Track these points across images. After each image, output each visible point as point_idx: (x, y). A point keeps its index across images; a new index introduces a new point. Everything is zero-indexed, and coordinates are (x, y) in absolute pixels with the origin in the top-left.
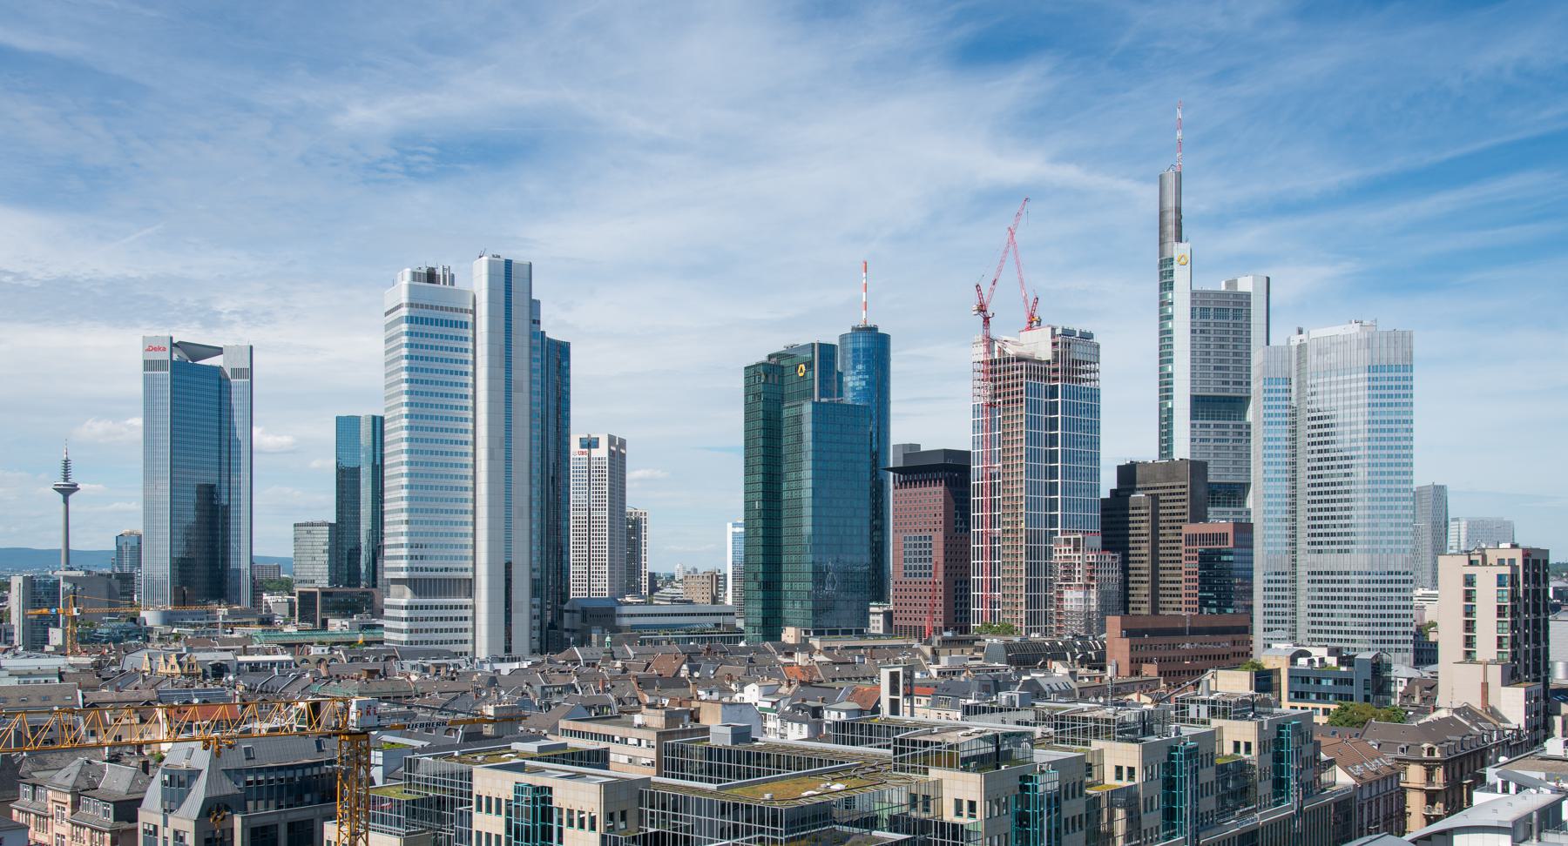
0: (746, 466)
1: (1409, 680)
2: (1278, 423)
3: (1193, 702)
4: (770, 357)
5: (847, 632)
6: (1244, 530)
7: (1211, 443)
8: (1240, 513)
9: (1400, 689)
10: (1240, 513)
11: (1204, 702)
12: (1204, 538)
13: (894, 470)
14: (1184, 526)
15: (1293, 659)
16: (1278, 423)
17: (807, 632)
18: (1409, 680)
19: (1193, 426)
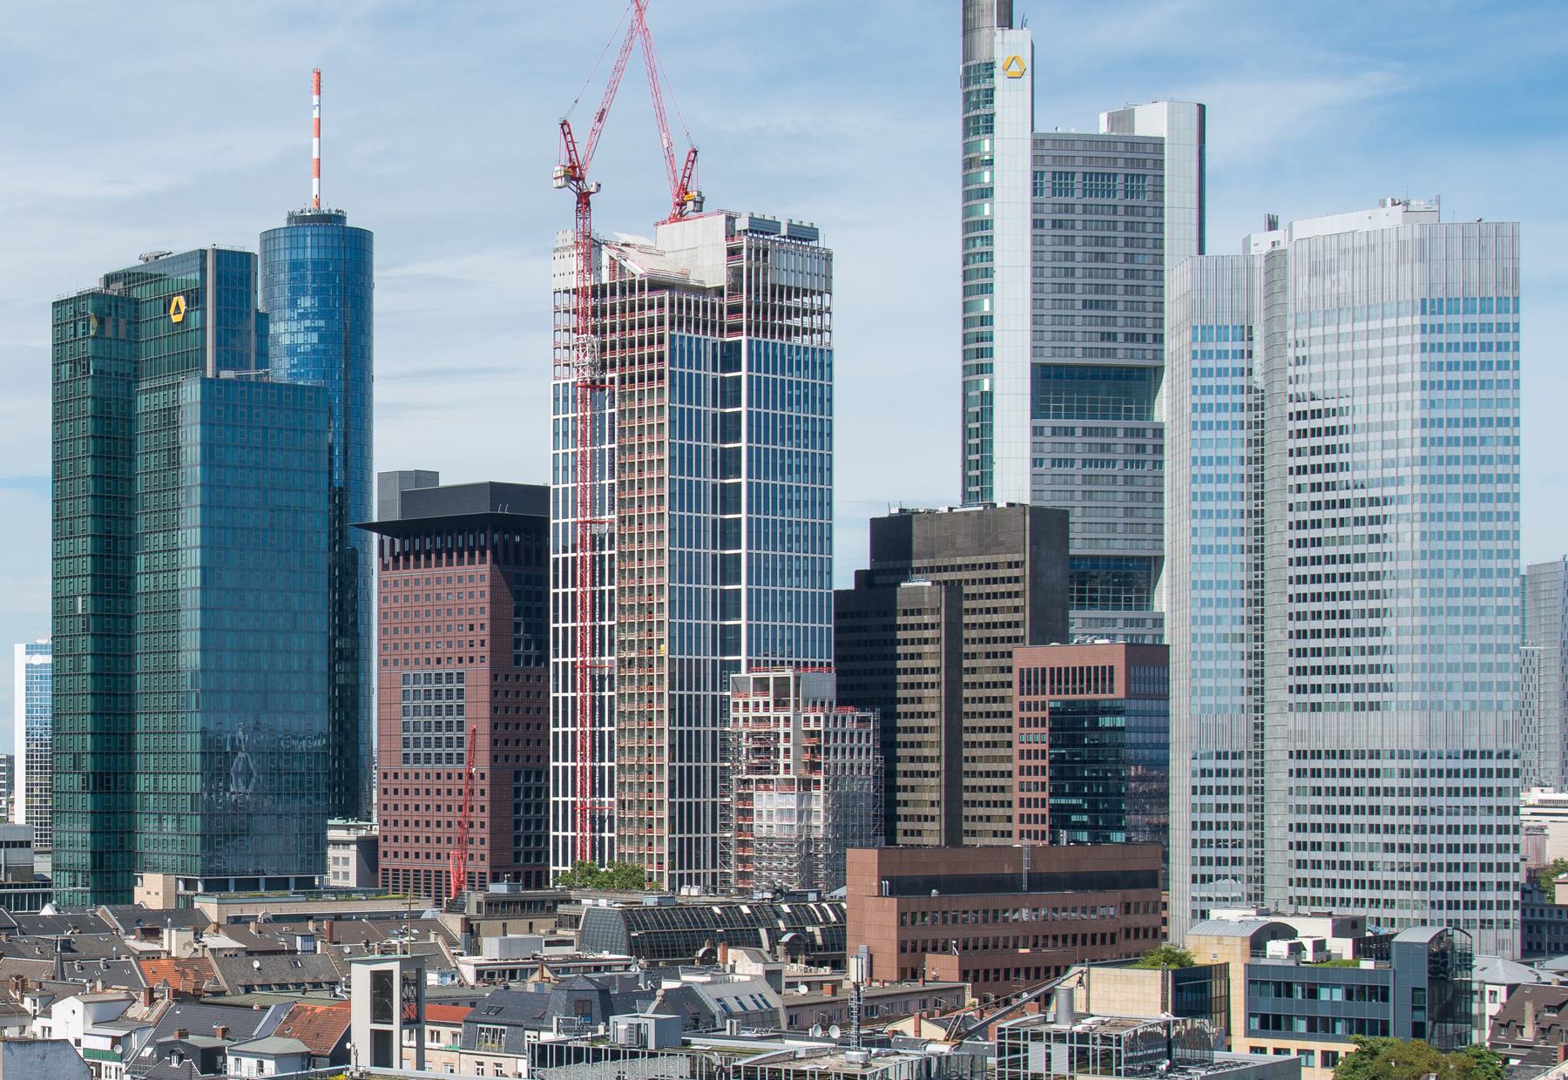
1: (1511, 989)
3: (1037, 1037)
4: (109, 279)
5: (278, 884)
6: (1149, 661)
7: (1077, 469)
8: (1139, 623)
9: (1492, 1009)
10: (1139, 623)
11: (1060, 1037)
12: (1061, 677)
13: (380, 528)
17: (189, 884)
18: (1511, 989)
19: (1036, 431)
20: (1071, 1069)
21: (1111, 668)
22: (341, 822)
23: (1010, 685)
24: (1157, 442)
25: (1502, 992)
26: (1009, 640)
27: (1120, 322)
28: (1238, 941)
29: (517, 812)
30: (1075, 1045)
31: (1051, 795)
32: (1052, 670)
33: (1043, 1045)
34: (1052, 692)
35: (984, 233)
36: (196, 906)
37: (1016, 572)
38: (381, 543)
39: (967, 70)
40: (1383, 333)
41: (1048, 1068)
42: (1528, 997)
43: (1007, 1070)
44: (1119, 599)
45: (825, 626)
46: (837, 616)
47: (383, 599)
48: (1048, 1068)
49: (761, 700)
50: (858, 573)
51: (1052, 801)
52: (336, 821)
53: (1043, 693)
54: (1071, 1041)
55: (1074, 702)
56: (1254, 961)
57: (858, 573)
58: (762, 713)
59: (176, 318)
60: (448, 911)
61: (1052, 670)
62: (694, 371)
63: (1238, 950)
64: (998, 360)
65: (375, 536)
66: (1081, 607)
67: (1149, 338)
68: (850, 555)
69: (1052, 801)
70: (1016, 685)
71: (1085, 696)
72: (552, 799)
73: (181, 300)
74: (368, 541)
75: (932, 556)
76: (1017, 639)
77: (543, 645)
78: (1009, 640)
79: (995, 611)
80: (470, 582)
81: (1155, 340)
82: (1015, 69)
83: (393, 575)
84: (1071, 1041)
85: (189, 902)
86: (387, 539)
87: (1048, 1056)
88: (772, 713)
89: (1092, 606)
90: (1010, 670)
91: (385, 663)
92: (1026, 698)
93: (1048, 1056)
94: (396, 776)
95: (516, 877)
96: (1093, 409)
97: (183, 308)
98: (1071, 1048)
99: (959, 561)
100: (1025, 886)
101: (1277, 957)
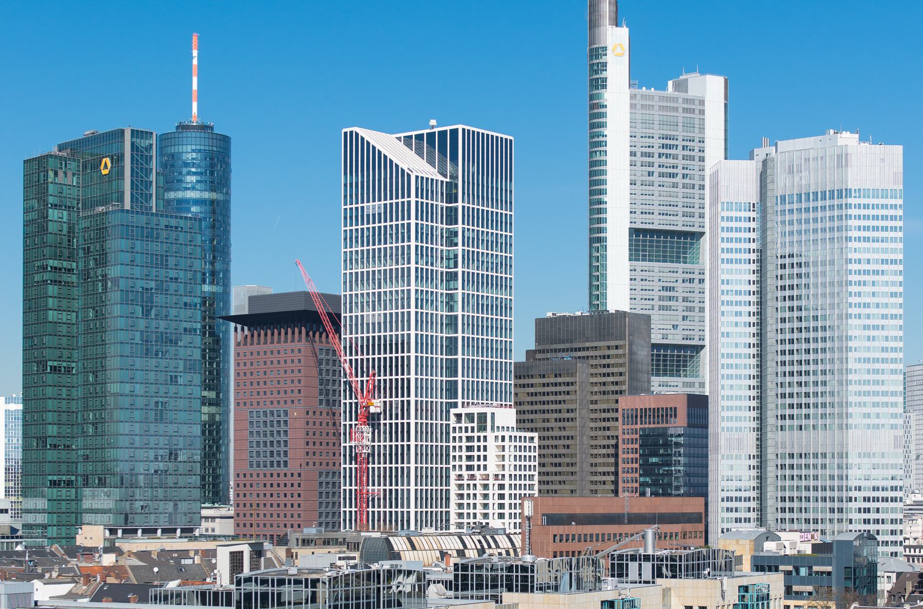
0: (26, 299)
1: (899, 575)
2: (738, 261)
3: (633, 558)
4: (61, 148)
5: (169, 531)
6: (698, 406)
7: (656, 160)
8: (691, 385)
9: (888, 587)
10: (691, 385)
11: (647, 558)
12: (644, 414)
13: (237, 319)
14: (620, 398)
15: (758, 543)
16: (738, 261)
17: (113, 531)
18: (899, 575)
19: (633, 97)
20: (653, 577)
21: (675, 408)
22: (210, 505)
23: (617, 419)
24: (701, 108)
25: (894, 576)
26: (617, 392)
27: (680, 195)
28: (748, 542)
29: (321, 497)
30: (656, 563)
31: (641, 475)
32: (641, 409)
33: (636, 564)
34: (641, 424)
35: (602, 149)
36: (117, 545)
37: (621, 361)
38: (236, 329)
39: (591, 50)
40: (823, 208)
41: (640, 565)
42: (909, 579)
43: (616, 562)
44: (679, 257)
45: (508, 382)
46: (516, 377)
47: (237, 393)
48: (640, 565)
49: (470, 425)
50: (528, 352)
51: (642, 479)
52: (207, 505)
53: (636, 424)
54: (653, 560)
55: (654, 429)
56: (757, 554)
57: (528, 352)
58: (470, 434)
59: (105, 172)
60: (278, 545)
61: (641, 409)
62: (429, 355)
63: (748, 547)
64: (610, 187)
65: (233, 325)
66: (658, 375)
67: (697, 112)
68: (522, 342)
69: (642, 479)
70: (620, 419)
71: (660, 425)
72: (342, 509)
73: (108, 160)
74: (227, 332)
75: (572, 342)
76: (621, 392)
77: (337, 435)
78: (617, 392)
79: (608, 366)
80: (293, 348)
81: (700, 104)
82: (618, 51)
83: (242, 348)
84: (653, 560)
85: (113, 542)
86: (239, 326)
87: (640, 575)
88: (476, 434)
89: (665, 375)
90: (617, 410)
91: (238, 404)
92: (625, 427)
93: (640, 575)
94: (245, 475)
95: (320, 524)
96: (664, 256)
97: (109, 165)
98: (653, 565)
99: (587, 345)
100: (626, 521)
101: (770, 551)
